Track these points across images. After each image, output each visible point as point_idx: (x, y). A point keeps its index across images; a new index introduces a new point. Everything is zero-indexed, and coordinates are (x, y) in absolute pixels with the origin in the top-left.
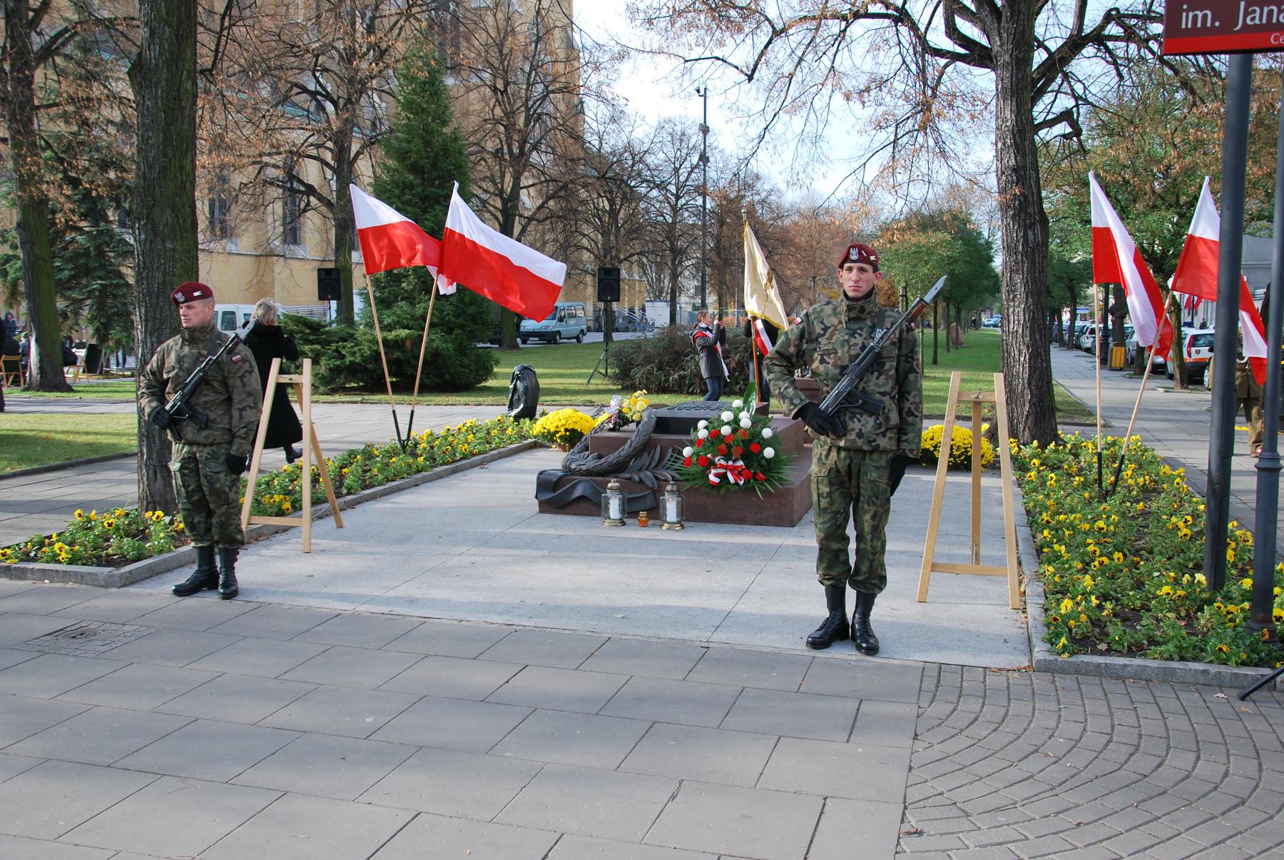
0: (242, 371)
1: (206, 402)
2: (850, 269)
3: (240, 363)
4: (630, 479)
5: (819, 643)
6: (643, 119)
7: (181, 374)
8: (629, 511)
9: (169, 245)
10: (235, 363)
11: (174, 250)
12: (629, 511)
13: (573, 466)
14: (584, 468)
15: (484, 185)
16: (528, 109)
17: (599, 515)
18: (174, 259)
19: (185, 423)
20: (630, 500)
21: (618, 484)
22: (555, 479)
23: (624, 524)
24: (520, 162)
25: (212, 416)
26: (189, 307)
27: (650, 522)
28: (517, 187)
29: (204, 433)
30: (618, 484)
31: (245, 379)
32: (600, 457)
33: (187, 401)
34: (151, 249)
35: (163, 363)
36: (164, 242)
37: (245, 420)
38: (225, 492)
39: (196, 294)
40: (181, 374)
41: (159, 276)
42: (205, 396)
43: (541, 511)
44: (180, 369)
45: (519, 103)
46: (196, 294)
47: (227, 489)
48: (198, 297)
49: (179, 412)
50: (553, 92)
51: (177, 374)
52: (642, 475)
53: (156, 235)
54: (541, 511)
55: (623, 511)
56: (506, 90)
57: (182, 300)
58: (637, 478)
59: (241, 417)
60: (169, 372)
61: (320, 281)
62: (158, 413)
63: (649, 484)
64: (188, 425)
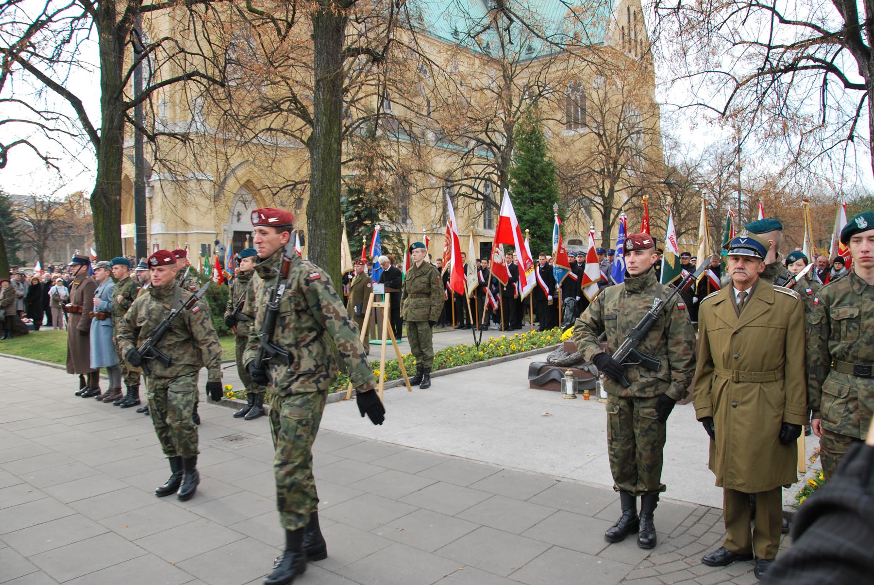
0: (202, 318)
1: (170, 345)
2: (859, 240)
3: (199, 313)
4: (582, 369)
5: (615, 538)
6: (694, 146)
7: (151, 323)
8: (579, 388)
9: (323, 232)
10: (195, 313)
11: (326, 234)
12: (579, 388)
13: (551, 360)
14: (556, 361)
15: (592, 190)
16: (618, 145)
17: (559, 391)
18: (326, 239)
19: (154, 363)
20: (580, 383)
21: (571, 372)
22: (539, 368)
23: (575, 397)
24: (614, 178)
25: (175, 356)
26: (159, 270)
27: (591, 397)
28: (612, 191)
29: (170, 369)
30: (571, 372)
31: (205, 325)
32: (569, 354)
33: (155, 345)
34: (315, 234)
35: (136, 314)
36: (321, 230)
37: (213, 354)
38: (179, 409)
39: (167, 260)
40: (151, 323)
41: (318, 248)
42: (170, 340)
43: (531, 387)
44: (150, 320)
45: (614, 142)
46: (167, 260)
47: (181, 407)
48: (168, 263)
49: (149, 353)
50: (633, 134)
51: (147, 323)
52: (590, 367)
53: (317, 226)
54: (531, 387)
55: (574, 389)
56: (604, 134)
57: (155, 264)
58: (586, 369)
59: (210, 352)
60: (141, 322)
61: (481, 249)
62: (133, 354)
63: (593, 373)
64: (156, 364)
